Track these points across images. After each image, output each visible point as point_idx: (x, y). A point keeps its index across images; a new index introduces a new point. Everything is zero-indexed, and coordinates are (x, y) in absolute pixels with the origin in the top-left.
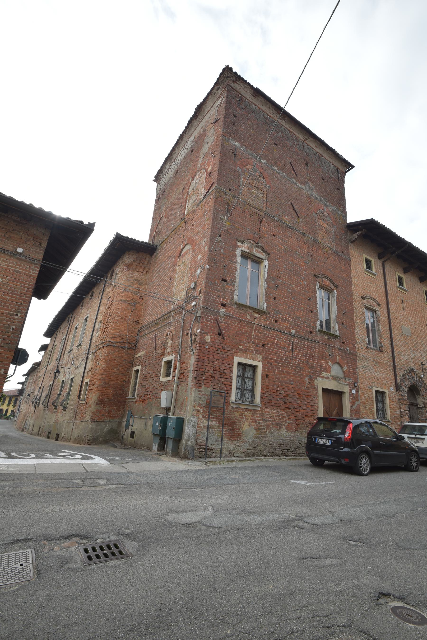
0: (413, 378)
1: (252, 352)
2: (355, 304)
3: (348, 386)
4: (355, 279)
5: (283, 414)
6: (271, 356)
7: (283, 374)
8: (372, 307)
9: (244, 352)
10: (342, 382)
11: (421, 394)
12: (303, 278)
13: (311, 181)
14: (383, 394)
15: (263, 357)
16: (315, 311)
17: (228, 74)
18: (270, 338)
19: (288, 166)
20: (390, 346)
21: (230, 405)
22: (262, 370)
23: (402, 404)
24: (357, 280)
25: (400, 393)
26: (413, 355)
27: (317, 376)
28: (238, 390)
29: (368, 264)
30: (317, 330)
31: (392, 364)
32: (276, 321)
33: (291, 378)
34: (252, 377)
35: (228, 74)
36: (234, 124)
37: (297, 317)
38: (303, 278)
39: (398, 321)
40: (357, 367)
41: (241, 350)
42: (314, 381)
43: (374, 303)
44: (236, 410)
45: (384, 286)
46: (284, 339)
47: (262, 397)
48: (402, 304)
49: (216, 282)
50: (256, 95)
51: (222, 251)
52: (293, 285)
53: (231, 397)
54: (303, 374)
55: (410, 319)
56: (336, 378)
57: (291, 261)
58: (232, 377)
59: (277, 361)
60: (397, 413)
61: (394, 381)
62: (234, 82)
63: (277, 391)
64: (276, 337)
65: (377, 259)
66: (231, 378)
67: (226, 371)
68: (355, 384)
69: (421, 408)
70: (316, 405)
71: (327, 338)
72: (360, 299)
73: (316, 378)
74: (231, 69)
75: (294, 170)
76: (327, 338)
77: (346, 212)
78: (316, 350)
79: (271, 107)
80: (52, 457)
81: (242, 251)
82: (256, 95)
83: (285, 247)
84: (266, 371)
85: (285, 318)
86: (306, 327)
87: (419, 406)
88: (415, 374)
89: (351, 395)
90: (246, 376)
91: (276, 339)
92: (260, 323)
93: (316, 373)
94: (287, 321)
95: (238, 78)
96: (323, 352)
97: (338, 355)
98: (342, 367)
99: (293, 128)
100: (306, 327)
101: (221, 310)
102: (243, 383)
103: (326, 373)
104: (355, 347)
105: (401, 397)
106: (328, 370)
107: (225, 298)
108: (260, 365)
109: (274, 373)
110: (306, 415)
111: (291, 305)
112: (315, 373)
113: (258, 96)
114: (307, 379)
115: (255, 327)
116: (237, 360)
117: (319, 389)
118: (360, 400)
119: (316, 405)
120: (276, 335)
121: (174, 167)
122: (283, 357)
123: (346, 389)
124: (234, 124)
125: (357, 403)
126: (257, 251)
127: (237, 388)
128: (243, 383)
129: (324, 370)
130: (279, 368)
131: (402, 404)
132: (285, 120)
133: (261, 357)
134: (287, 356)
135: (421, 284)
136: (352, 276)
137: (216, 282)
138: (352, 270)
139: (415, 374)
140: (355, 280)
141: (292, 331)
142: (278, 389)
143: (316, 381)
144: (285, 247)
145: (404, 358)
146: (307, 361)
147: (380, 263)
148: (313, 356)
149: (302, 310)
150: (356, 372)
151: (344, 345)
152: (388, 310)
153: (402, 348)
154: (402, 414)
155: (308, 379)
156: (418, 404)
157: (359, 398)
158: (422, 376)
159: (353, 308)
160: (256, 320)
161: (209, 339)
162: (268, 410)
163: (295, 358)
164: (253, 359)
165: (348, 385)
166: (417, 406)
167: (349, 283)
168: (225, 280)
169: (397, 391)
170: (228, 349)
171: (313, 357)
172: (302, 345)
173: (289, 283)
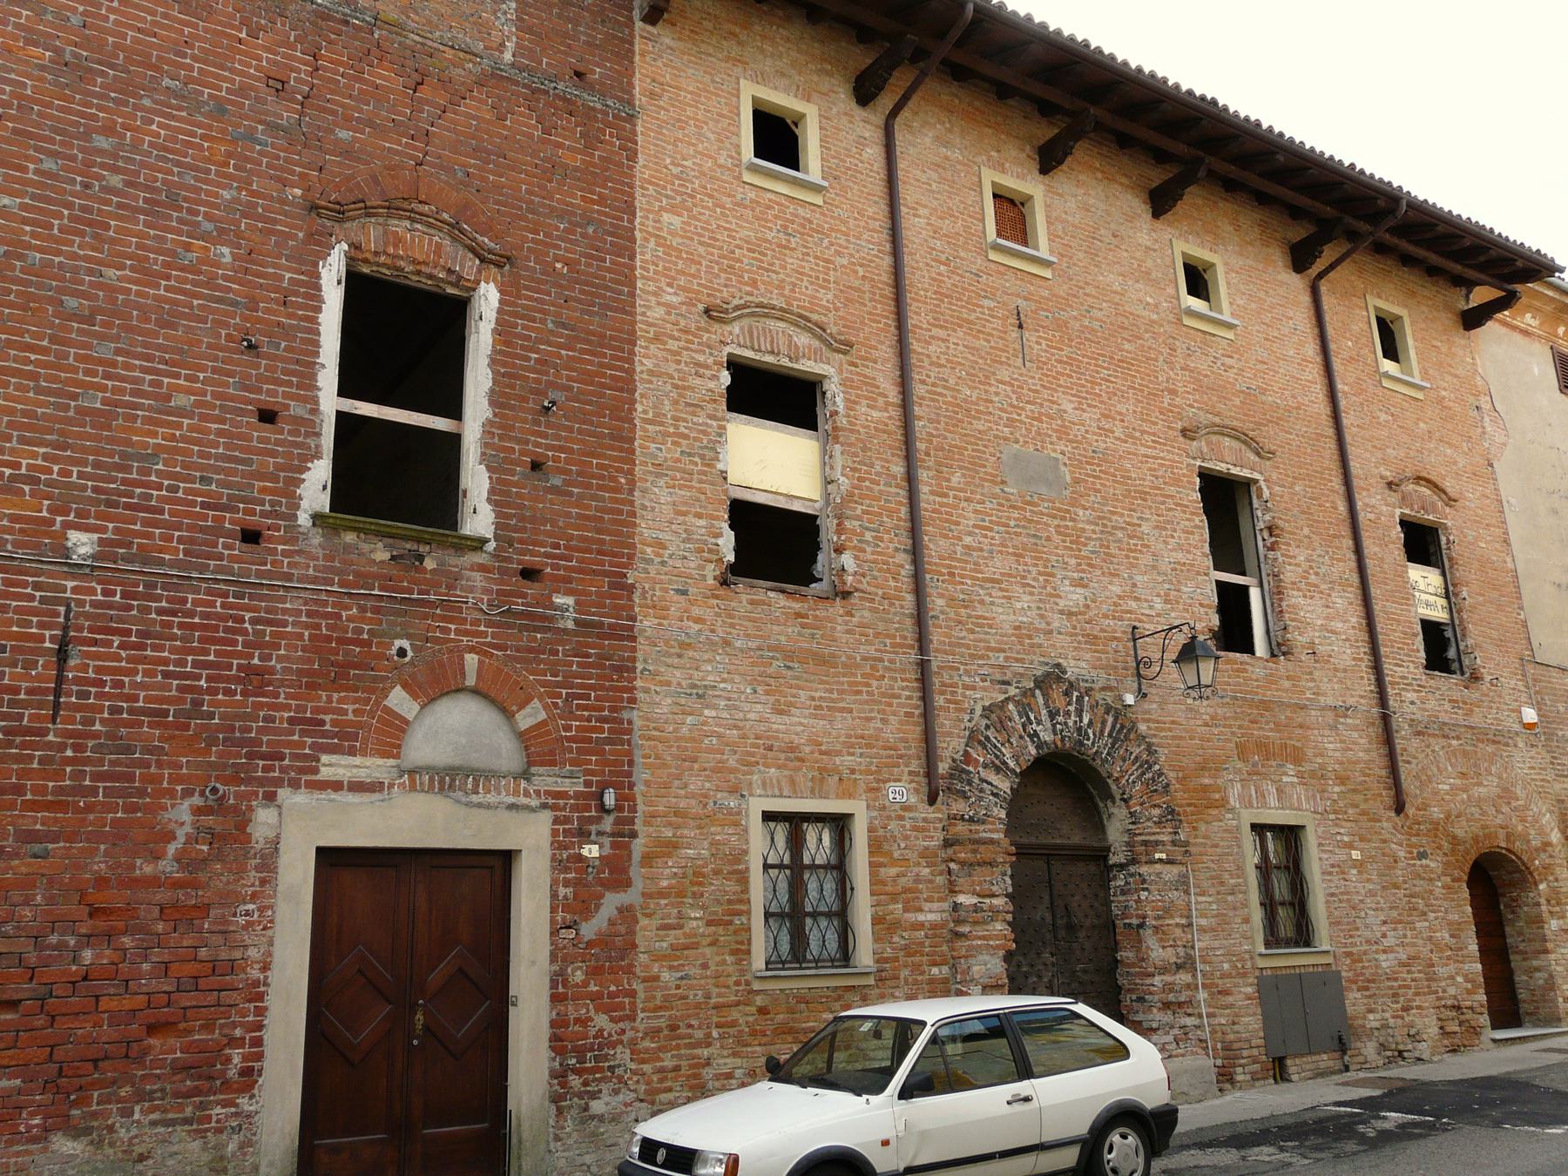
0: (1052, 715)
3: (546, 817)
4: (666, 217)
8: (785, 362)
10: (491, 798)
11: (1118, 797)
14: (1290, 835)
16: (296, 409)
20: (903, 559)
23: (962, 863)
25: (959, 807)
26: (1074, 597)
27: (278, 783)
28: (771, 921)
29: (777, 139)
31: (913, 656)
34: (833, 862)
39: (979, 425)
43: (803, 340)
45: (888, 247)
48: (1015, 334)
55: (1069, 407)
56: (447, 780)
60: (931, 917)
61: (915, 748)
65: (843, 98)
68: (602, 795)
69: (1122, 867)
70: (253, 953)
71: (382, 555)
72: (695, 319)
76: (382, 555)
83: (58, 51)
87: (1113, 860)
88: (1067, 693)
90: (807, 861)
93: (266, 769)
97: (472, 650)
98: (508, 715)
102: (797, 888)
105: (961, 828)
111: (82, 384)
114: (181, 814)
117: (284, 859)
118: (638, 885)
119: (253, 953)
121: (1421, 253)
123: (531, 838)
125: (611, 903)
127: (768, 915)
128: (797, 888)
131: (962, 863)
135: (1158, 224)
139: (1067, 693)
140: (658, 225)
144: (56, 50)
145: (1004, 618)
147: (864, 126)
150: (622, 731)
151: (531, 590)
152: (902, 376)
153: (998, 566)
154: (958, 922)
156: (1108, 849)
157: (636, 872)
158: (1130, 699)
165: (544, 806)
166: (1106, 858)
169: (932, 800)
171: (256, 679)
173: (74, 256)
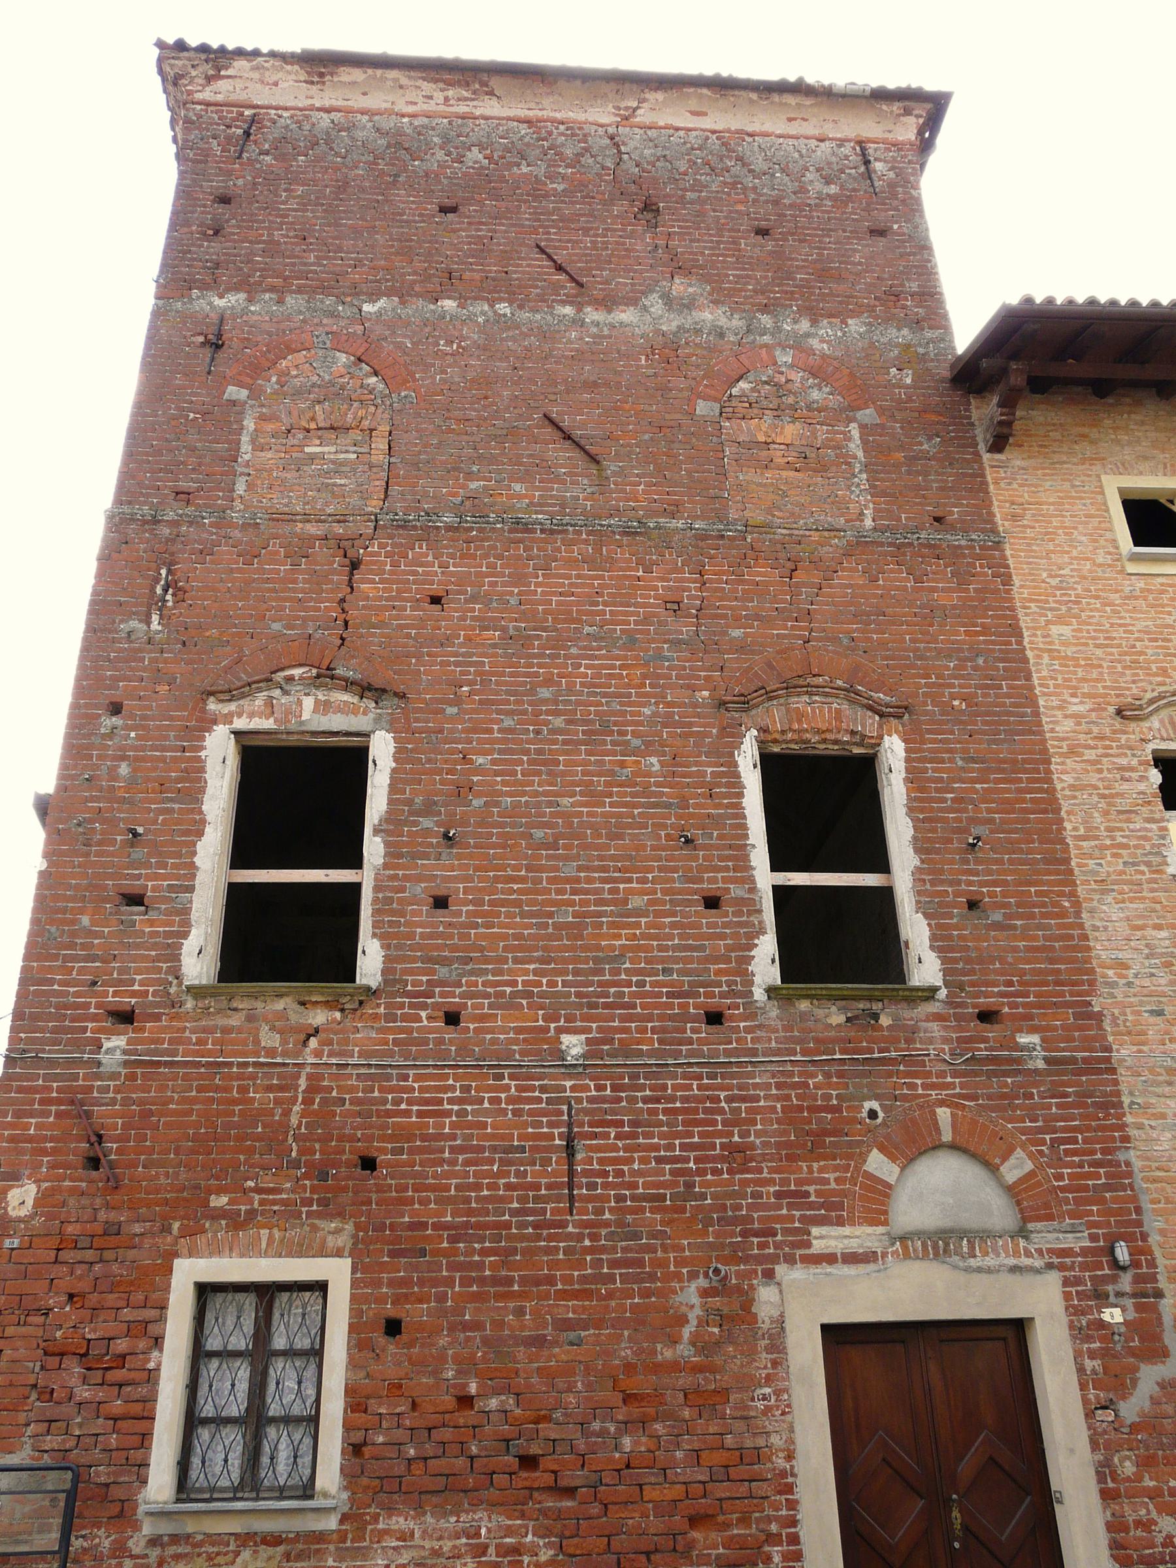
1: (290, 1213)
2: (1065, 775)
5: (509, 1531)
6: (413, 1214)
7: (510, 1296)
9: (237, 1222)
12: (636, 742)
13: (678, 267)
15: (358, 1227)
16: (736, 891)
17: (172, 66)
18: (407, 1113)
19: (532, 265)
21: (136, 1526)
22: (353, 1298)
24: (1066, 631)
27: (775, 1259)
30: (759, 994)
32: (452, 1019)
33: (569, 1310)
35: (172, 66)
36: (216, 232)
37: (596, 960)
38: (636, 742)
40: (1126, 1139)
41: (217, 1215)
42: (747, 1304)
44: (172, 1550)
46: (509, 1101)
47: (354, 1450)
49: (85, 920)
50: (321, 75)
51: (124, 769)
52: (566, 801)
53: (145, 1482)
54: (663, 1264)
56: (941, 1244)
57: (548, 682)
58: (158, 1369)
59: (458, 1234)
62: (209, 79)
63: (466, 1401)
64: (451, 1101)
66: (152, 1377)
67: (121, 1345)
71: (837, 1018)
72: (1107, 723)
73: (769, 1275)
74: (181, 46)
75: (559, 268)
77: (945, 316)
78: (756, 1110)
79: (404, 81)
80: (279, 736)
81: (237, 734)
82: (321, 75)
83: (504, 629)
84: (381, 1300)
85: (514, 983)
86: (669, 995)
89: (1086, 1330)
91: (448, 1113)
92: (341, 1054)
93: (762, 1246)
94: (530, 995)
95: (217, 59)
96: (813, 1109)
97: (942, 1103)
99: (546, 102)
100: (669, 995)
101: (107, 1045)
103: (847, 1230)
104: (1099, 1017)
106: (875, 1202)
107: (132, 982)
108: (337, 1272)
109: (441, 1298)
110: (695, 1521)
112: (755, 1244)
113: (332, 74)
114: (690, 1296)
115: (310, 1077)
116: (188, 1272)
119: (775, 1440)
120: (452, 1088)
122: (502, 1200)
123: (1042, 1302)
124: (216, 232)
126: (323, 707)
129: (833, 1211)
130: (480, 1266)
132: (491, 93)
133: (349, 1227)
134: (536, 1187)
136: (1024, 622)
137: (85, 920)
138: (1020, 589)
140: (1048, 639)
141: (567, 1039)
142: (473, 1388)
143: (766, 1295)
146: (690, 1186)
148: (740, 1149)
149: (638, 913)
150: (1120, 1176)
151: (992, 1032)
155: (705, 1293)
159: (1052, 791)
160: (313, 1043)
161: (30, 1203)
162: (399, 1523)
163: (592, 1186)
164: (300, 1250)
165: (1050, 1266)
167: (1005, 657)
168: (135, 900)
170: (137, 1228)
171: (739, 1157)
172: (646, 1100)
